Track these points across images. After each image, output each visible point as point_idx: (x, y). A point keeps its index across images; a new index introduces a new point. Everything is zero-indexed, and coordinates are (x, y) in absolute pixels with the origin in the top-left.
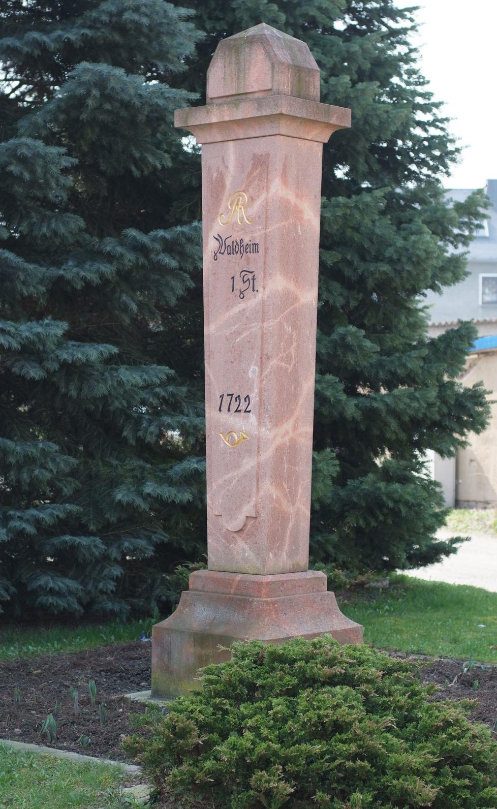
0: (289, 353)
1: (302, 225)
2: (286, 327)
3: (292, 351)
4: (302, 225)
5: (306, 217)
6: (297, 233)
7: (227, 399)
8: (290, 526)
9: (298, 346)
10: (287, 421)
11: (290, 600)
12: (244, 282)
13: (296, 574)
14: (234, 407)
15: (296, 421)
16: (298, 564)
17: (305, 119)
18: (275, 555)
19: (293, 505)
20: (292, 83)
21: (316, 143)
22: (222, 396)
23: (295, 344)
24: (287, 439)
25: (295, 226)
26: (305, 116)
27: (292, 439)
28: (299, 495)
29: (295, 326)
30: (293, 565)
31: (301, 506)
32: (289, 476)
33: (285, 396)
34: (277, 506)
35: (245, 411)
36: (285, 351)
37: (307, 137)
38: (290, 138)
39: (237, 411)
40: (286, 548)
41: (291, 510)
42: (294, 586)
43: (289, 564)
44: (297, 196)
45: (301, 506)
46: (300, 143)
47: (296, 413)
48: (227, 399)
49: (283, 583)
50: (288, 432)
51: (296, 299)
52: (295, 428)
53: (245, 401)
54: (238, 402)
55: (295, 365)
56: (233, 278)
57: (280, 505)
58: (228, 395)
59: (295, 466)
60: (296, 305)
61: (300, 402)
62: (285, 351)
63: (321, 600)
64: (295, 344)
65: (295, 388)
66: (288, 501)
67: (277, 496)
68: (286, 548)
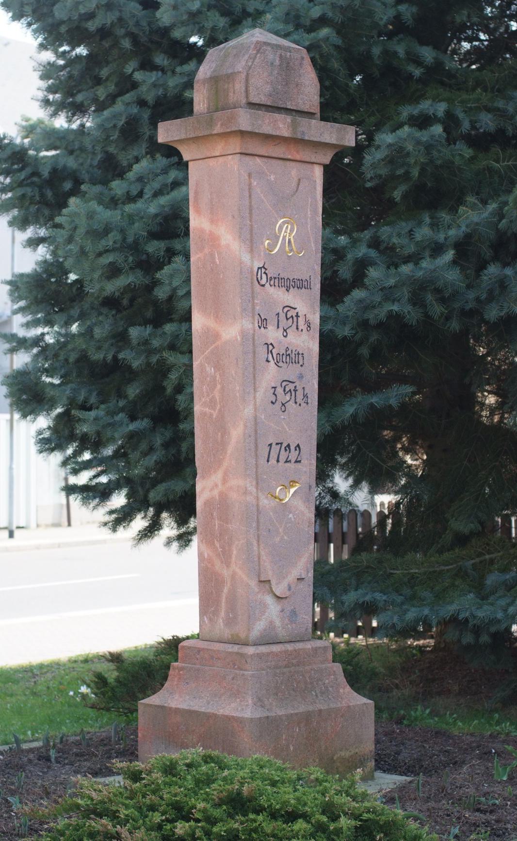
0: (213, 397)
1: (219, 254)
2: (208, 369)
3: (217, 394)
4: (219, 254)
5: (223, 242)
6: (214, 262)
7: (275, 449)
8: (226, 590)
9: (223, 388)
10: (215, 472)
11: (198, 670)
12: (287, 319)
13: (222, 644)
14: (283, 458)
15: (226, 474)
16: (237, 635)
17: (193, 138)
18: (211, 620)
19: (227, 566)
20: (208, 98)
21: (230, 157)
22: (270, 445)
23: (219, 387)
24: (216, 492)
25: (212, 255)
26: (183, 136)
27: (221, 494)
28: (234, 556)
29: (218, 367)
30: (232, 635)
31: (238, 571)
32: (221, 534)
33: (211, 445)
34: (209, 565)
35: (296, 462)
36: (208, 395)
37: (214, 154)
38: (200, 161)
39: (286, 462)
40: (223, 614)
41: (226, 573)
42: (212, 657)
43: (227, 633)
44: (212, 221)
45: (238, 571)
46: (212, 162)
47: (225, 464)
48: (275, 449)
49: (199, 650)
50: (216, 485)
51: (217, 336)
52: (225, 481)
53: (286, 450)
54: (297, 452)
55: (220, 410)
56: (278, 314)
57: (213, 565)
58: (277, 444)
59: (227, 523)
60: (218, 343)
61: (229, 452)
62: (208, 395)
63: (233, 679)
64: (219, 387)
65: (222, 437)
66: (222, 562)
67: (208, 555)
68: (223, 614)
